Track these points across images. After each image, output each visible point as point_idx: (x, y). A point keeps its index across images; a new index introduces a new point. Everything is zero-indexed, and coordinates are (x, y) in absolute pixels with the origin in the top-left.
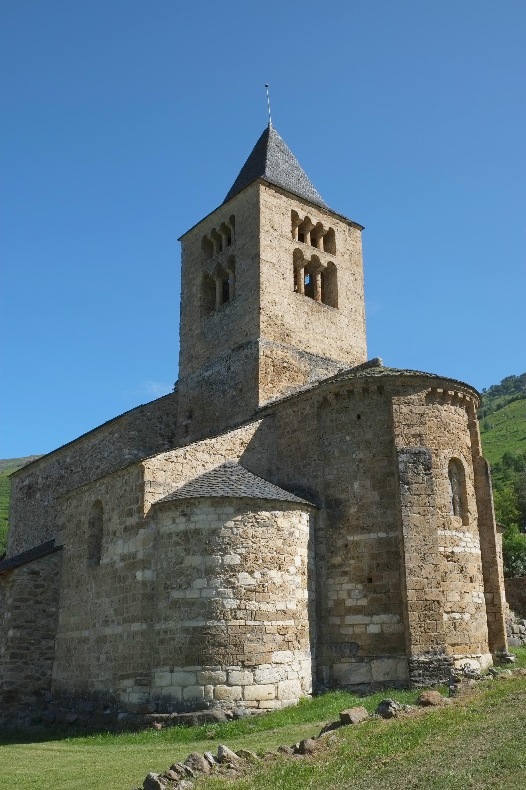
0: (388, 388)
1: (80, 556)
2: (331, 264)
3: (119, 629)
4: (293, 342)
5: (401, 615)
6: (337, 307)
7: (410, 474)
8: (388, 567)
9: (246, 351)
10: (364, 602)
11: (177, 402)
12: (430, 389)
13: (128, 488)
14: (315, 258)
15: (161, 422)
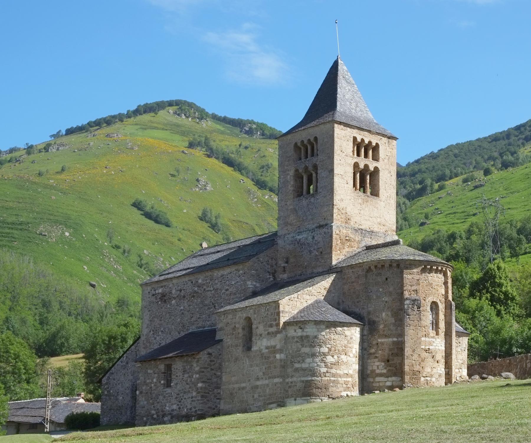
0: (402, 266)
1: (237, 346)
2: (376, 169)
3: (267, 382)
4: (352, 223)
5: (402, 377)
6: (379, 196)
7: (410, 310)
8: (397, 355)
9: (325, 230)
10: (385, 371)
11: (278, 251)
12: (423, 266)
13: (269, 313)
14: (366, 166)
15: (268, 264)
